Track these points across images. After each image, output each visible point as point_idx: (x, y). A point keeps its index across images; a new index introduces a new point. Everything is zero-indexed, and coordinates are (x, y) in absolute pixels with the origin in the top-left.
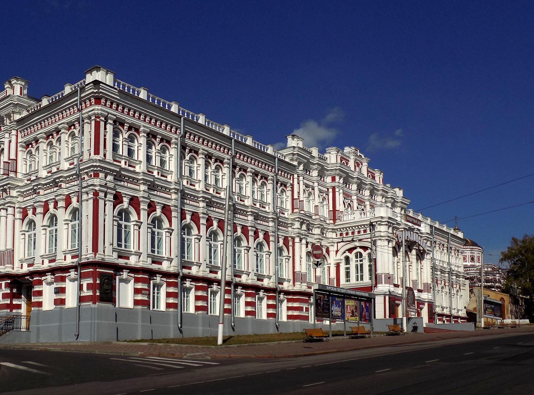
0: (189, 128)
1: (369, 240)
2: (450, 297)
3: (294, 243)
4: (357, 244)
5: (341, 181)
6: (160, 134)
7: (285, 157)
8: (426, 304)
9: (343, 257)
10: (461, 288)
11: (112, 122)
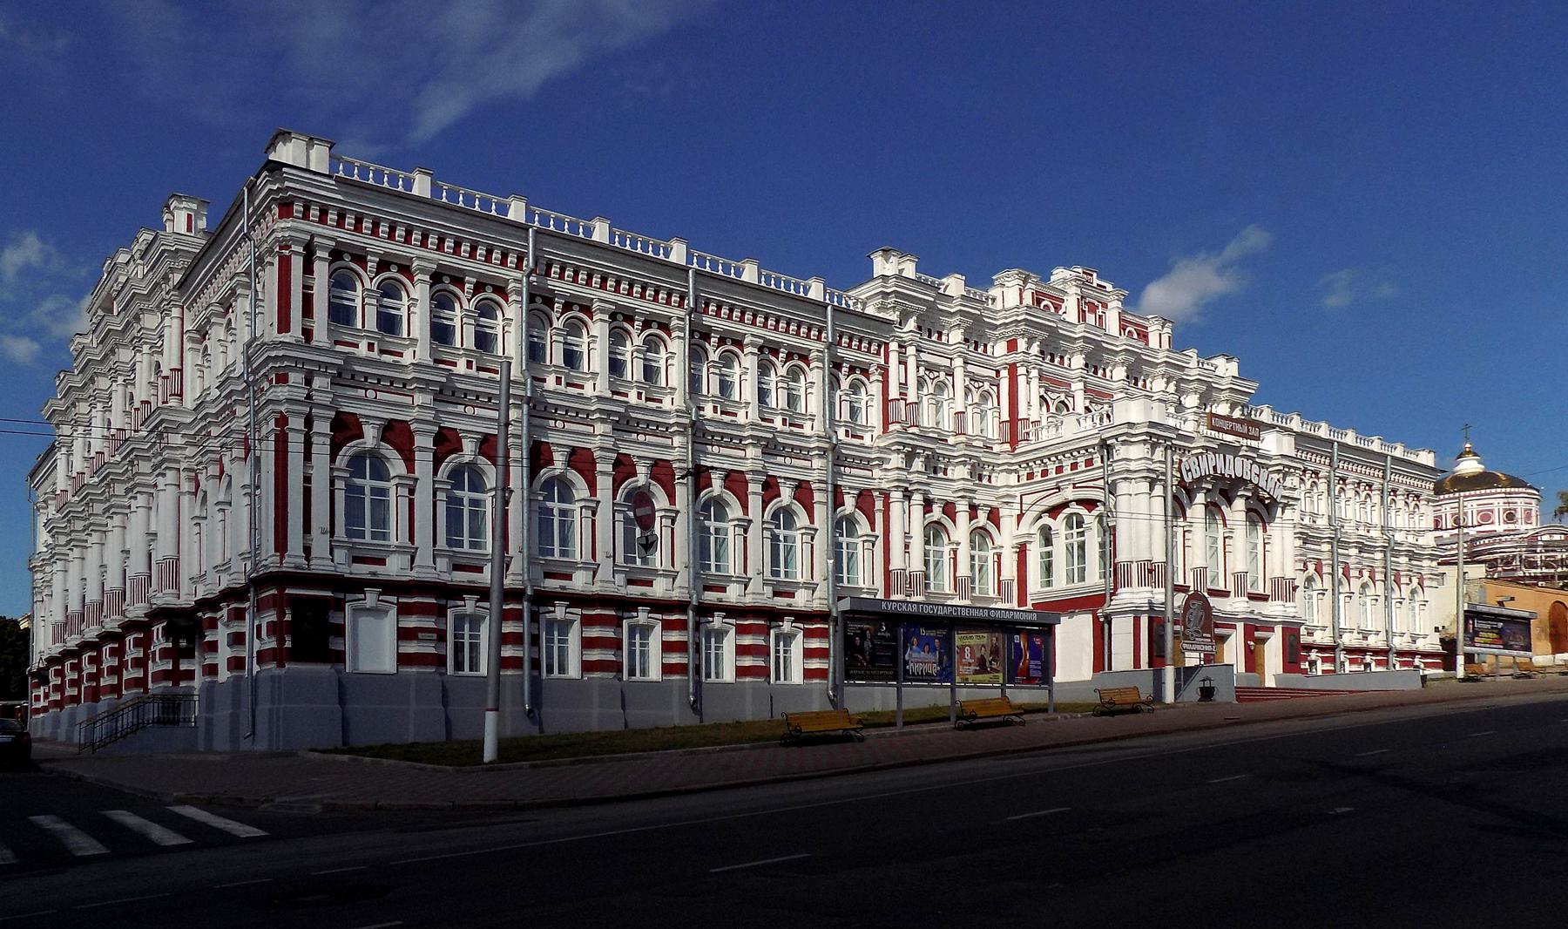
0: (551, 252)
1: (1101, 483)
2: (1388, 606)
3: (887, 505)
4: (1069, 493)
5: (1035, 349)
6: (472, 274)
7: (864, 304)
8: (1278, 629)
9: (1035, 529)
10: (1426, 583)
11: (326, 255)
